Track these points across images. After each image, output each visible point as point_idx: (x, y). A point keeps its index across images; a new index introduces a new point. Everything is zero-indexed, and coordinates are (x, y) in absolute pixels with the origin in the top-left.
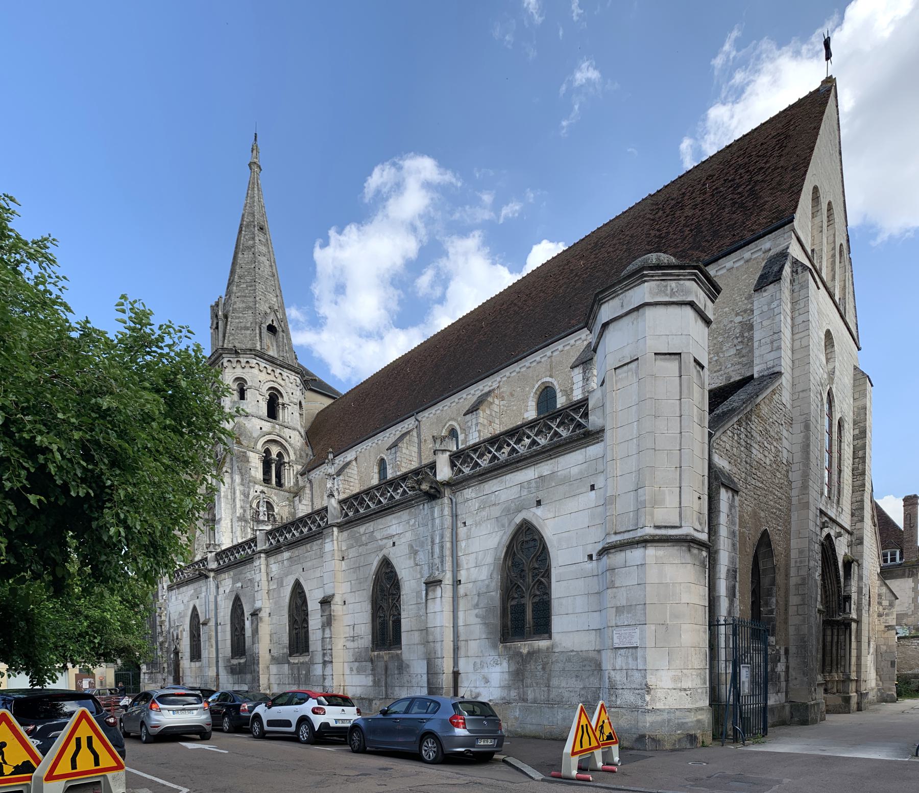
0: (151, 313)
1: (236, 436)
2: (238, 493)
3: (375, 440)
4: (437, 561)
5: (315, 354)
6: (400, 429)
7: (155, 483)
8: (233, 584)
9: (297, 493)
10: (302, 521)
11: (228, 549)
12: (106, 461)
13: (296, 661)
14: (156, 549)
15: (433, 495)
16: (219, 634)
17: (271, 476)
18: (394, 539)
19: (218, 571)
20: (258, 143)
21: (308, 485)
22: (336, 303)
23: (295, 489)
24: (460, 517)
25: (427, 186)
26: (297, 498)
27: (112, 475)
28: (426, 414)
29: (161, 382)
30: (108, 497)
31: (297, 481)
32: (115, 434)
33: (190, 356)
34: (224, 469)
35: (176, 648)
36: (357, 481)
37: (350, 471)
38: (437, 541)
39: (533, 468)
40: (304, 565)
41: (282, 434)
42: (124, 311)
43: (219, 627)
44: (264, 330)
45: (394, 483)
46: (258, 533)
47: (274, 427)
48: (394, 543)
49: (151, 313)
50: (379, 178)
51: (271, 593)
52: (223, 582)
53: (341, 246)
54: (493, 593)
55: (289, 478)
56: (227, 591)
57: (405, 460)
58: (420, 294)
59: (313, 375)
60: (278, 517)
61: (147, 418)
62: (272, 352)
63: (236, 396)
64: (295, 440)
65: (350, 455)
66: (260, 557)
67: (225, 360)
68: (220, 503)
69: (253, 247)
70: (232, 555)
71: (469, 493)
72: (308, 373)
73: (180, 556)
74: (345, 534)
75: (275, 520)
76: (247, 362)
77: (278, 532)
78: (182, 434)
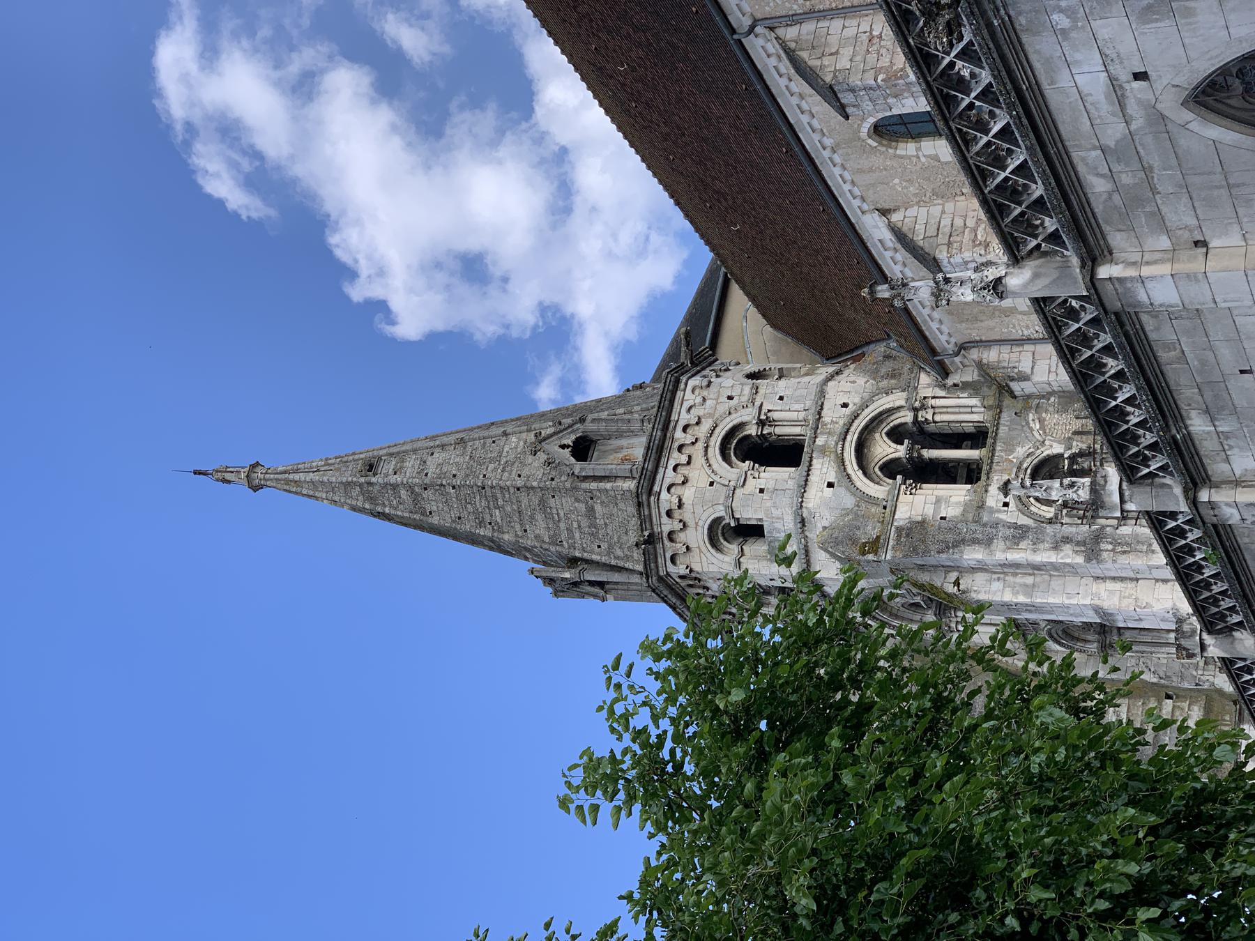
0: (588, 752)
1: (857, 548)
2: (1014, 556)
3: (822, 157)
5: (632, 335)
6: (783, 82)
7: (1001, 799)
9: (999, 387)
10: (1084, 374)
11: (1191, 593)
12: (954, 917)
14: (1199, 819)
17: (958, 461)
18: (1124, 76)
20: (209, 468)
21: (974, 354)
22: (505, 280)
23: (990, 392)
25: (209, 54)
26: (1016, 387)
27: (991, 911)
29: (740, 749)
30: (1052, 931)
31: (965, 386)
32: (881, 886)
33: (670, 671)
34: (951, 589)
36: (949, 206)
37: (920, 228)
41: (839, 428)
42: (595, 808)
44: (588, 468)
45: (943, 88)
46: (1131, 506)
47: (823, 450)
48: (1140, 76)
49: (588, 752)
50: (222, 185)
53: (381, 272)
55: (959, 409)
57: (872, 58)
58: (446, 49)
59: (676, 340)
60: (1078, 445)
61: (832, 800)
62: (636, 448)
63: (755, 548)
64: (849, 391)
65: (875, 230)
66: (1212, 505)
68: (1052, 608)
69: (410, 488)
70: (1208, 586)
72: (672, 354)
73: (1218, 753)
74: (1117, 239)
75: (1088, 453)
76: (669, 514)
77: (1123, 448)
78: (865, 707)
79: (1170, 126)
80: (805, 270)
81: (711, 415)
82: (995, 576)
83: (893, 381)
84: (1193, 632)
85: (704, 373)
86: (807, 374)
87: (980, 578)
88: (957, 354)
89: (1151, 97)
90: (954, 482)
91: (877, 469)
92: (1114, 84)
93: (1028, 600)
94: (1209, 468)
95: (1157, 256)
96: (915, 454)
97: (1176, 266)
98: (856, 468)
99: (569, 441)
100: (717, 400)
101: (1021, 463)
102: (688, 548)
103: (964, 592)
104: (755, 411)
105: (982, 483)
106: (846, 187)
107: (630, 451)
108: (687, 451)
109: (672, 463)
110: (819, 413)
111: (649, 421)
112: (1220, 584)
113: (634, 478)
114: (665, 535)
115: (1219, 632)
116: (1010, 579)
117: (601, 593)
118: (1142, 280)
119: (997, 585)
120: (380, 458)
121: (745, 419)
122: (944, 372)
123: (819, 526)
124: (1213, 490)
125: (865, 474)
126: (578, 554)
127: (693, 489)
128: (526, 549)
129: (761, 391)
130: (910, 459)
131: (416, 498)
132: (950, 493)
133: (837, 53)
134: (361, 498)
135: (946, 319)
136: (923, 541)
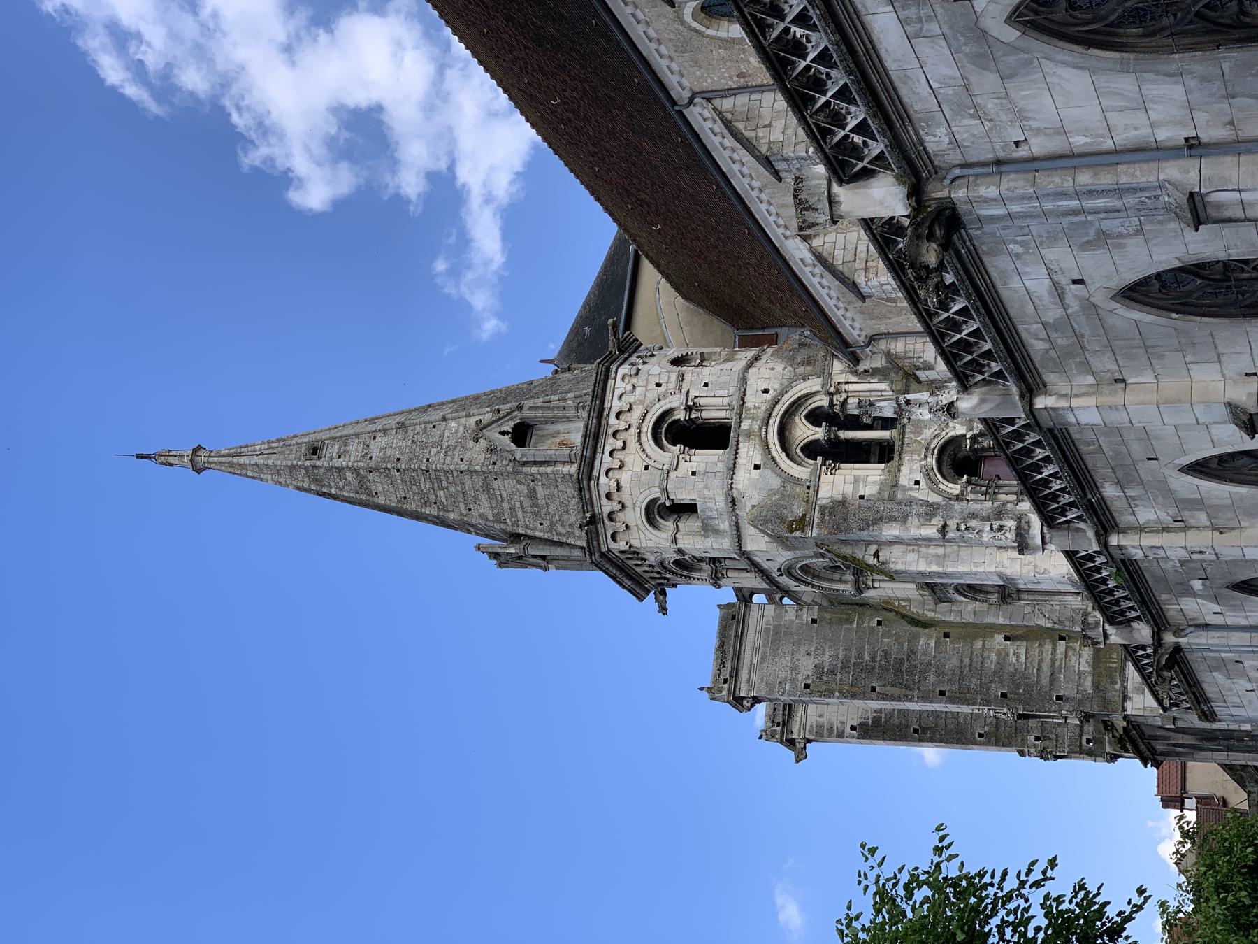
4: (1131, 200)
8: (1194, 594)
15: (945, 223)
17: (870, 442)
19: (1159, 624)
21: (883, 345)
23: (897, 377)
24: (1002, 155)
26: (919, 373)
28: (672, 80)
31: (874, 372)
34: (872, 561)
37: (839, 253)
38: (1074, 203)
39: (868, 19)
41: (761, 413)
47: (748, 434)
48: (1075, 282)
51: (1221, 523)
52: (1191, 615)
54: (1226, 66)
56: (1217, 608)
62: (575, 434)
63: (689, 524)
66: (1120, 547)
67: (612, 545)
69: (356, 471)
71: (936, 141)
74: (1050, 378)
77: (1045, 505)
79: (1100, 311)
80: (723, 266)
81: (642, 402)
83: (809, 368)
84: (1097, 623)
86: (728, 360)
87: (897, 549)
88: (868, 345)
90: (867, 461)
92: (1055, 285)
93: (940, 570)
95: (1084, 389)
96: (833, 436)
97: (1101, 399)
98: (780, 450)
99: (508, 427)
101: (929, 445)
102: (627, 527)
103: (883, 563)
104: (683, 397)
105: (894, 463)
106: (772, 219)
107: (567, 436)
108: (621, 436)
109: (608, 449)
110: (743, 399)
111: (584, 408)
113: (572, 463)
114: (605, 515)
115: (1120, 623)
116: (923, 550)
117: (543, 563)
118: (1072, 409)
119: (912, 557)
120: (323, 442)
121: (674, 405)
122: (855, 359)
123: (749, 505)
125: (788, 455)
126: (521, 531)
127: (629, 473)
128: (472, 526)
129: (687, 378)
131: (362, 481)
132: (867, 472)
133: (770, 125)
134: (306, 480)
135: (858, 317)
136: (846, 520)
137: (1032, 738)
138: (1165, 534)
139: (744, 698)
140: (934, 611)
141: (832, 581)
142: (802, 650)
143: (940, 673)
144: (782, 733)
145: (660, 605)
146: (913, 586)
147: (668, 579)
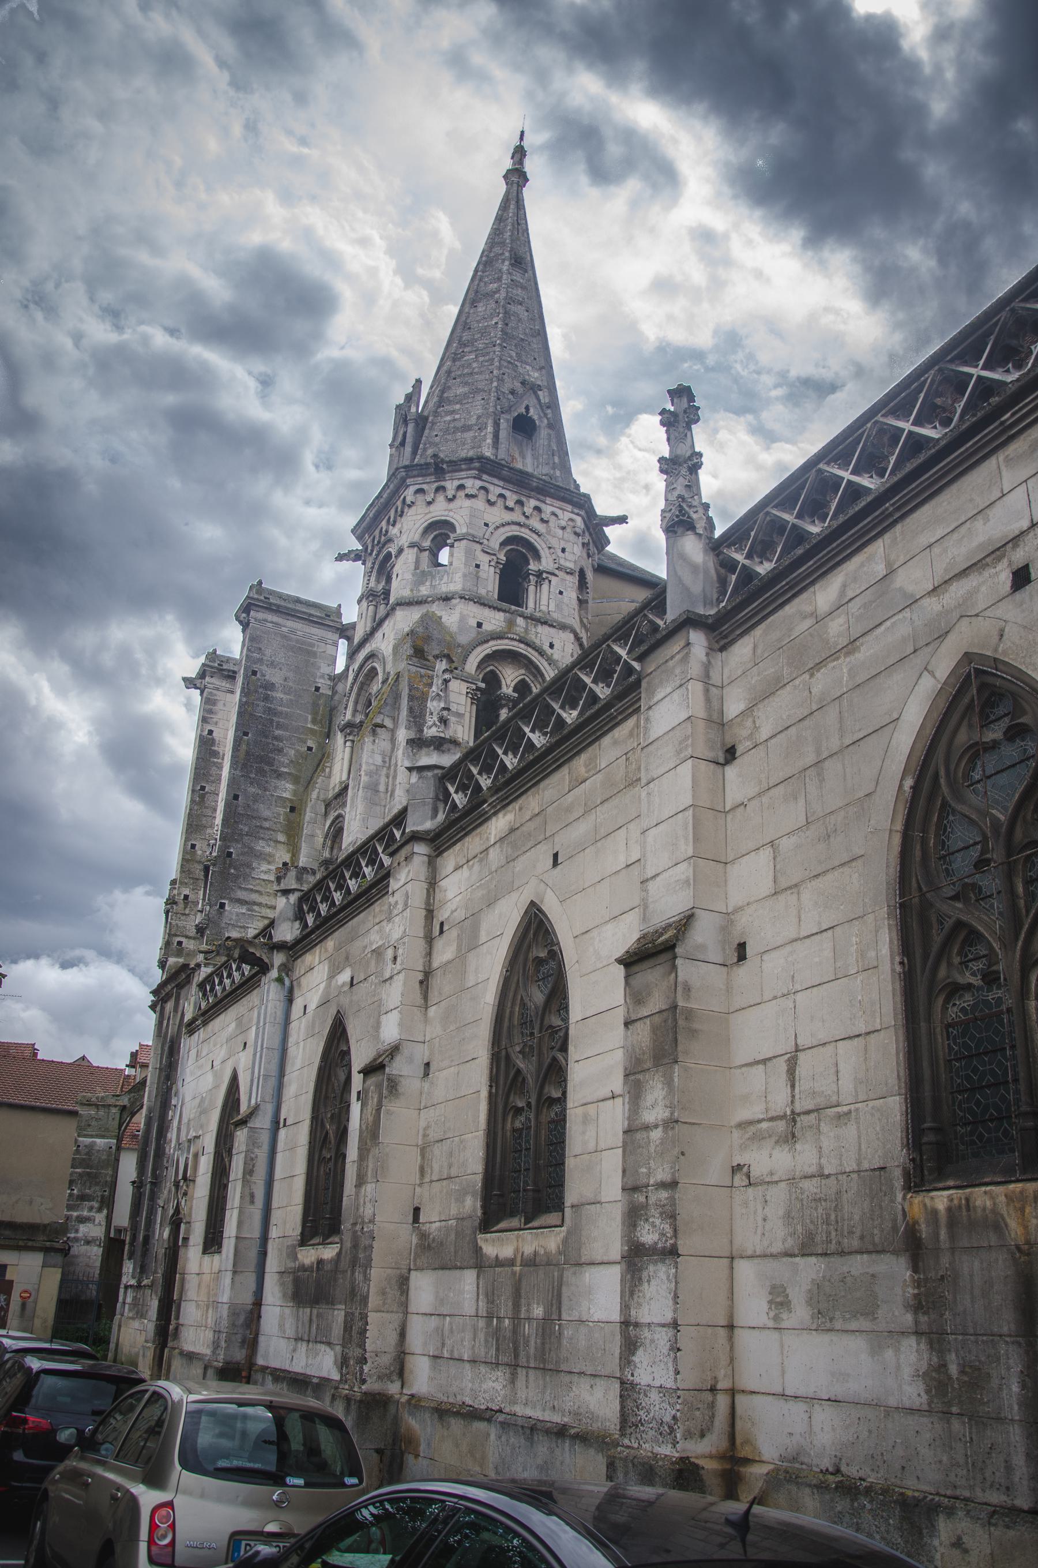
8: (331, 977)
13: (507, 1251)
16: (279, 1158)
35: (177, 1211)
40: (563, 841)
41: (532, 637)
43: (282, 1133)
47: (511, 623)
56: (312, 1007)
67: (412, 489)
81: (549, 532)
82: (387, 759)
85: (587, 534)
89: (981, 606)
91: (492, 667)
94: (451, 850)
95: (716, 704)
98: (494, 649)
100: (563, 539)
109: (507, 493)
112: (340, 898)
114: (443, 483)
117: (397, 444)
120: (526, 271)
121: (543, 560)
124: (426, 859)
129: (568, 577)
130: (500, 698)
137: (187, 892)
138: (424, 913)
139: (248, 615)
140: (318, 798)
141: (356, 702)
142: (291, 675)
143: (256, 798)
144: (212, 667)
145: (345, 555)
146: (344, 777)
147: (371, 554)
